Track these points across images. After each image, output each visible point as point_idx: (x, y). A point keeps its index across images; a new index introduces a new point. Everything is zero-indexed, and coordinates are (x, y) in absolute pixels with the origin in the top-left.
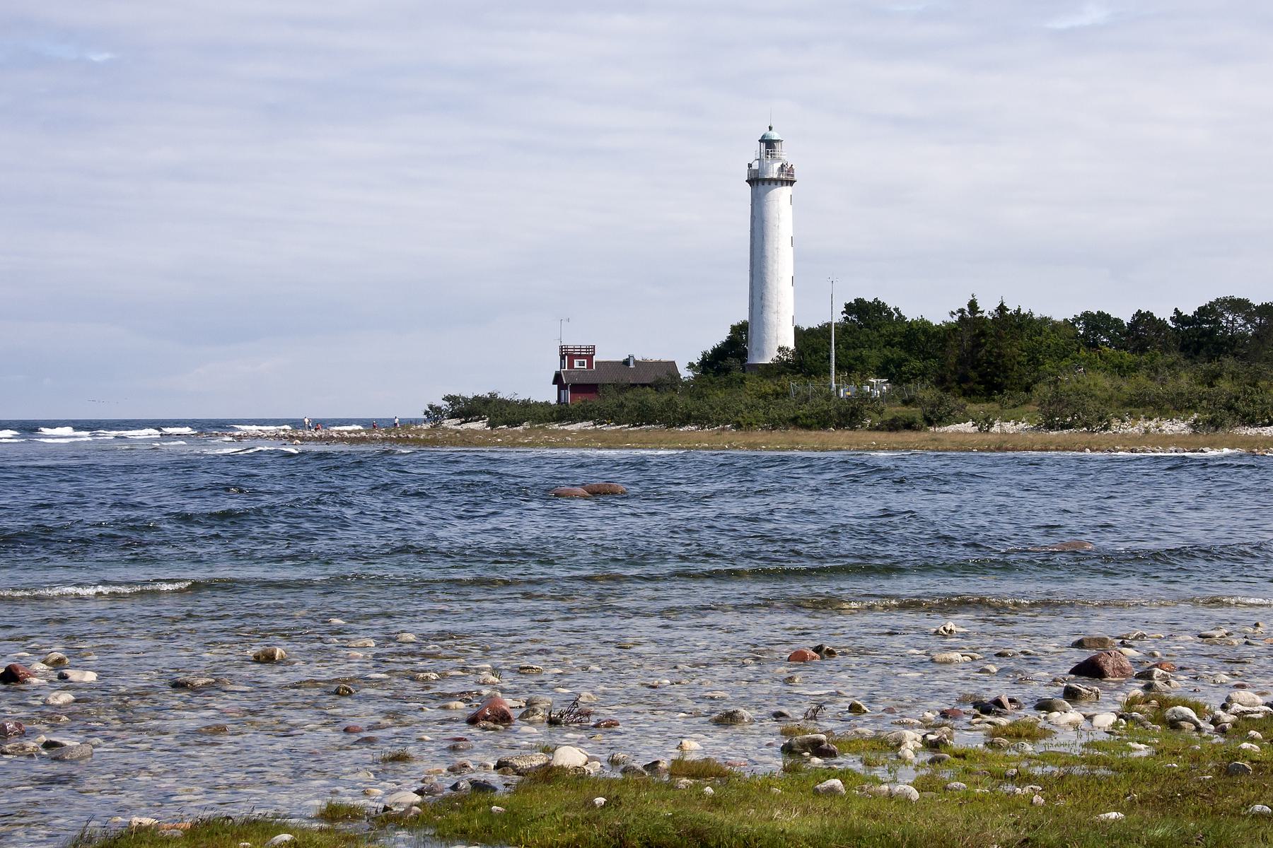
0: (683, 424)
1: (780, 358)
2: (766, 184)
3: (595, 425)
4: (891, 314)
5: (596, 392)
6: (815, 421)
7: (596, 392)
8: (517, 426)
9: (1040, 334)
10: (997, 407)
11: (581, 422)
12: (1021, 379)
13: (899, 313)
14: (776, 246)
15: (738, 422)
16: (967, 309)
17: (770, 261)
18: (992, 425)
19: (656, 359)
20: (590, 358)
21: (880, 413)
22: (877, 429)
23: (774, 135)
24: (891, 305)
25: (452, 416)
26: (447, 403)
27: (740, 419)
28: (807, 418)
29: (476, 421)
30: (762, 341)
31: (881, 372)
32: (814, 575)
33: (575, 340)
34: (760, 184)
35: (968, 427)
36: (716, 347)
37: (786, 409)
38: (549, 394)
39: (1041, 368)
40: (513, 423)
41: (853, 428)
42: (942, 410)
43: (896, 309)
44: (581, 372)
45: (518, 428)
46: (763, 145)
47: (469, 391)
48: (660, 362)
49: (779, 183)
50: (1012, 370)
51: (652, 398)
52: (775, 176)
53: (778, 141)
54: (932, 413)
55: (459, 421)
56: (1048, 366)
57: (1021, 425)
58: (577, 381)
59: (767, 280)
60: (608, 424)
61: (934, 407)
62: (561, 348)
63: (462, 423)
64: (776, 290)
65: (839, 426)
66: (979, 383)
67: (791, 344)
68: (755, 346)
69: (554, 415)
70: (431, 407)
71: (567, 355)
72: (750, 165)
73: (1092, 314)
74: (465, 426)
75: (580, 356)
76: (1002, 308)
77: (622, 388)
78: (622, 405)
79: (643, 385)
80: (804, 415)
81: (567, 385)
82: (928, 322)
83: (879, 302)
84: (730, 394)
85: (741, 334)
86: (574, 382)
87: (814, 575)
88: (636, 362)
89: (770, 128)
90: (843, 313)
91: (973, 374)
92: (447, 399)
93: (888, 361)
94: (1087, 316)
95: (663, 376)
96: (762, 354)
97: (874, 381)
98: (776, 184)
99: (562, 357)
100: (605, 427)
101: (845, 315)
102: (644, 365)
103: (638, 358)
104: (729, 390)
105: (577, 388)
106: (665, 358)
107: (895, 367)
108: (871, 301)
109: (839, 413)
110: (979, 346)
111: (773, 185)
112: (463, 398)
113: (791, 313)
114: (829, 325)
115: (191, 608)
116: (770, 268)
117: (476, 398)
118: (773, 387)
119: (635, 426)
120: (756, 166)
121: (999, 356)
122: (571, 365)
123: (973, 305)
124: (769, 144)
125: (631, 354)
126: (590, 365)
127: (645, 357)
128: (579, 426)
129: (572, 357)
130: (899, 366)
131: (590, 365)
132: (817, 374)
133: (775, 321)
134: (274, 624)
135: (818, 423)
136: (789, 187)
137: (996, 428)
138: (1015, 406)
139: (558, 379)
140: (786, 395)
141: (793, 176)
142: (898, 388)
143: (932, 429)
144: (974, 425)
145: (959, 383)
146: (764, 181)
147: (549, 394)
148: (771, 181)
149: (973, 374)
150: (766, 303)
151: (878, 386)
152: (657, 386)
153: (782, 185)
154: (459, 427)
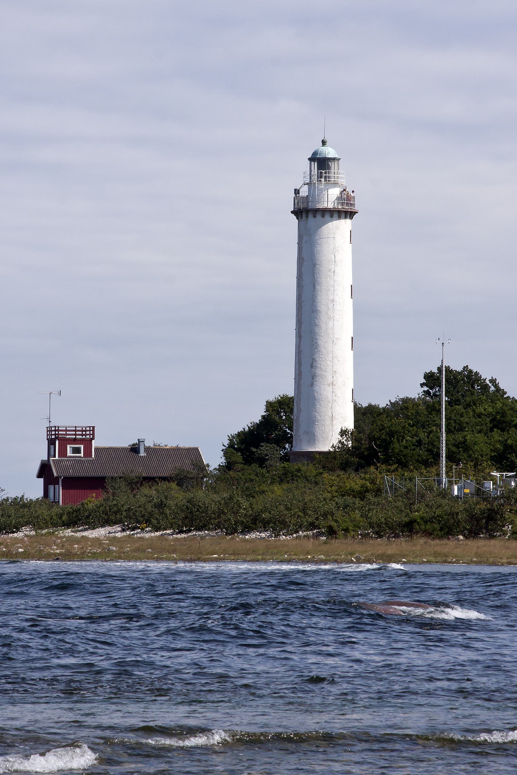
0: (247, 529)
1: (342, 443)
3: (123, 530)
4: (485, 387)
5: (104, 488)
6: (437, 526)
7: (104, 488)
8: (13, 532)
11: (102, 526)
13: (496, 386)
14: (331, 297)
17: (323, 318)
20: (88, 443)
23: (329, 152)
24: (486, 375)
27: (333, 524)
28: (426, 522)
30: (312, 422)
32: (331, 747)
34: (311, 216)
36: (247, 429)
43: (493, 381)
44: (79, 461)
45: (15, 535)
46: (315, 165)
48: (177, 450)
49: (336, 215)
52: (331, 206)
53: (334, 159)
58: (71, 473)
59: (321, 342)
60: (142, 529)
62: (49, 430)
64: (331, 355)
67: (350, 425)
72: (297, 192)
75: (75, 441)
79: (164, 479)
80: (422, 518)
81: (57, 478)
83: (471, 371)
84: (290, 490)
85: (279, 413)
86: (66, 475)
87: (331, 747)
88: (147, 449)
89: (324, 143)
90: (422, 385)
95: (187, 466)
96: (312, 439)
98: (332, 216)
99: (51, 442)
100: (138, 534)
101: (426, 388)
103: (149, 443)
104: (285, 486)
106: (185, 443)
111: (327, 216)
113: (350, 385)
114: (415, 398)
116: (323, 326)
119: (181, 532)
120: (304, 192)
122: (63, 452)
125: (141, 437)
127: (158, 442)
128: (100, 532)
129: (64, 442)
132: (426, 464)
133: (330, 395)
135: (441, 529)
136: (348, 221)
140: (378, 492)
141: (353, 205)
146: (316, 212)
150: (318, 372)
153: (339, 218)
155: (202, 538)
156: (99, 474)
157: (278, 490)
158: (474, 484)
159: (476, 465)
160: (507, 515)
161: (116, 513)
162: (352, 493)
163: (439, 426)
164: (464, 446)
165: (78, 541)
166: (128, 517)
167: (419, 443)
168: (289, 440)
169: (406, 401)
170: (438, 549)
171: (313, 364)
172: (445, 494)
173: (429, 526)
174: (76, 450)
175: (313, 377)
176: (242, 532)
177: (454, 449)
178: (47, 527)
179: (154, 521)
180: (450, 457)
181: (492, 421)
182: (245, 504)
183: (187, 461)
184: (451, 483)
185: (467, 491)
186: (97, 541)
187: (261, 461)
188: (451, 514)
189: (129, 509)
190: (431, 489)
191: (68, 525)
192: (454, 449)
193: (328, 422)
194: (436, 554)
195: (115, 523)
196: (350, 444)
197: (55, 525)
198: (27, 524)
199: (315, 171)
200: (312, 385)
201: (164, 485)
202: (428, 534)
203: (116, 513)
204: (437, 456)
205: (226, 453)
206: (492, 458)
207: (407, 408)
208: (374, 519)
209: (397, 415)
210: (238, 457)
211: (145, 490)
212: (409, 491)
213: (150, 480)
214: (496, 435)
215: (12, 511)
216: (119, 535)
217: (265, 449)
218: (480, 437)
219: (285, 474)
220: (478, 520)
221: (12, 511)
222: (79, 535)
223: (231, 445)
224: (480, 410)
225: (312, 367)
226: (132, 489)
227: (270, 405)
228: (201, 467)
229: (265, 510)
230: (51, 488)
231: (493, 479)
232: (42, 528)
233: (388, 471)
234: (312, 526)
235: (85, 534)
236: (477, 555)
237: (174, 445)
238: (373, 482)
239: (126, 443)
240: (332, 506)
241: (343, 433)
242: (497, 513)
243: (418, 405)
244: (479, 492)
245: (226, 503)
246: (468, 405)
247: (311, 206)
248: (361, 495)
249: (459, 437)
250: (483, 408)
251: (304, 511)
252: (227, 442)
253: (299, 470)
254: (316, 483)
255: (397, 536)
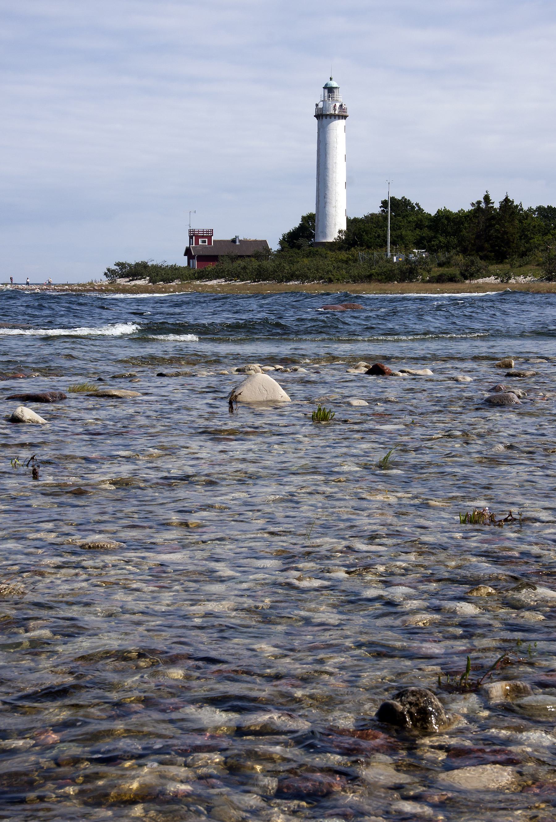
0: (288, 280)
2: (328, 118)
3: (226, 281)
4: (414, 207)
5: (217, 261)
9: (526, 219)
10: (508, 267)
12: (519, 248)
13: (419, 207)
15: (330, 278)
16: (483, 201)
18: (510, 278)
19: (253, 238)
20: (210, 238)
21: (429, 271)
22: (429, 281)
23: (334, 84)
24: (413, 201)
25: (122, 276)
26: (118, 268)
27: (331, 276)
29: (140, 279)
30: (325, 227)
31: (419, 244)
33: (200, 226)
35: (491, 280)
37: (360, 268)
38: (183, 262)
39: (531, 241)
40: (167, 280)
41: (411, 281)
42: (473, 269)
43: (417, 204)
44: (205, 247)
46: (326, 91)
47: (132, 259)
48: (256, 241)
49: (337, 117)
50: (513, 242)
51: (255, 263)
54: (466, 270)
55: (128, 280)
56: (537, 239)
57: (528, 278)
58: (201, 253)
59: (329, 185)
61: (468, 266)
63: (130, 281)
65: (402, 280)
66: (491, 252)
67: (344, 228)
68: (320, 230)
69: (196, 275)
70: (108, 270)
71: (194, 235)
72: (317, 105)
73: (544, 208)
74: (133, 283)
75: (203, 237)
76: (507, 200)
77: (234, 258)
78: (244, 268)
79: (249, 256)
80: (376, 273)
81: (194, 256)
82: (449, 211)
83: (406, 199)
84: (312, 261)
88: (240, 241)
89: (331, 79)
90: (380, 207)
91: (486, 245)
92: (118, 264)
93: (423, 238)
94: (540, 209)
95: (260, 250)
97: (416, 251)
99: (191, 237)
102: (244, 242)
103: (241, 238)
104: (309, 259)
105: (202, 258)
107: (427, 242)
108: (400, 198)
109: (401, 271)
110: (492, 226)
111: (333, 118)
112: (129, 265)
115: (293, 489)
116: (330, 176)
117: (137, 264)
118: (346, 256)
119: (255, 282)
120: (321, 105)
121: (505, 233)
123: (487, 199)
124: (330, 90)
126: (210, 243)
127: (246, 237)
128: (214, 282)
129: (198, 237)
130: (429, 241)
131: (210, 243)
132: (381, 246)
133: (334, 213)
134: (192, 466)
136: (344, 120)
137: (512, 281)
138: (520, 266)
139: (188, 252)
140: (355, 261)
142: (431, 256)
143: (467, 282)
144: (496, 279)
145: (477, 252)
146: (327, 116)
147: (183, 262)
148: (331, 116)
149: (486, 245)
150: (328, 200)
151: (416, 253)
152: (257, 256)
153: (339, 119)
154: (129, 283)
155: (265, 284)
156: (216, 254)
157: (306, 261)
158: (404, 256)
159: (405, 247)
160: (419, 271)
161: (222, 272)
162: (342, 261)
163: (387, 227)
164: (401, 237)
165: (201, 286)
166: (228, 274)
167: (379, 236)
168: (314, 237)
169: (372, 215)
170: (383, 287)
171: (325, 197)
172: (390, 261)
173: (380, 278)
174: (204, 242)
175: (325, 203)
176: (286, 282)
177: (395, 239)
178: (187, 280)
179: (241, 277)
180: (393, 243)
181: (416, 225)
182: (288, 268)
183: (261, 247)
184: (392, 255)
185: (401, 259)
186: (212, 286)
187: (299, 247)
188: (391, 271)
189: (228, 270)
190: (382, 259)
191: (198, 279)
192: (395, 239)
193: (333, 227)
194: (381, 290)
195: (222, 278)
196: (344, 237)
197: (191, 279)
198: (177, 278)
199: (326, 94)
200: (325, 207)
201: (247, 259)
202: (380, 281)
203: (222, 272)
204: (386, 242)
205: (281, 243)
206: (414, 243)
207: (373, 219)
208: (352, 274)
209: (368, 222)
210: (286, 245)
211: (239, 262)
212: (370, 259)
213: (241, 256)
214: (418, 232)
215: (170, 272)
216: (223, 283)
217: (301, 241)
218: (409, 233)
219: (310, 253)
220: (405, 273)
221: (170, 272)
222: (203, 283)
223: (284, 239)
224: (410, 219)
225: (325, 198)
226: (232, 262)
227: (304, 218)
228: (267, 250)
229: (298, 270)
230: (191, 261)
231: (414, 253)
232: (184, 280)
233: (361, 250)
234: (321, 278)
235: (206, 283)
236: (401, 290)
237: (254, 239)
238: (353, 256)
239: (229, 238)
240: (331, 268)
241: (340, 232)
242: (414, 269)
243: (378, 217)
244: (407, 261)
245: (278, 267)
246: (404, 217)
247: (324, 113)
248: (346, 262)
249: (398, 232)
250: (412, 218)
251: (317, 270)
252: (281, 238)
253: (317, 251)
254: (326, 258)
255: (363, 282)
